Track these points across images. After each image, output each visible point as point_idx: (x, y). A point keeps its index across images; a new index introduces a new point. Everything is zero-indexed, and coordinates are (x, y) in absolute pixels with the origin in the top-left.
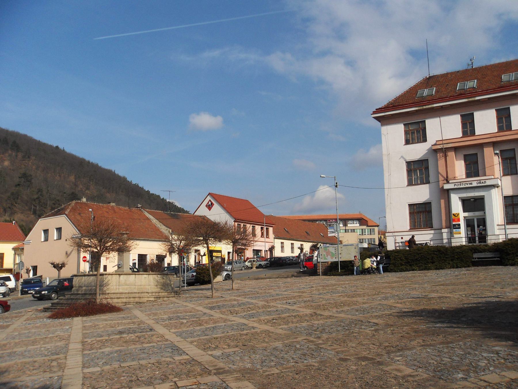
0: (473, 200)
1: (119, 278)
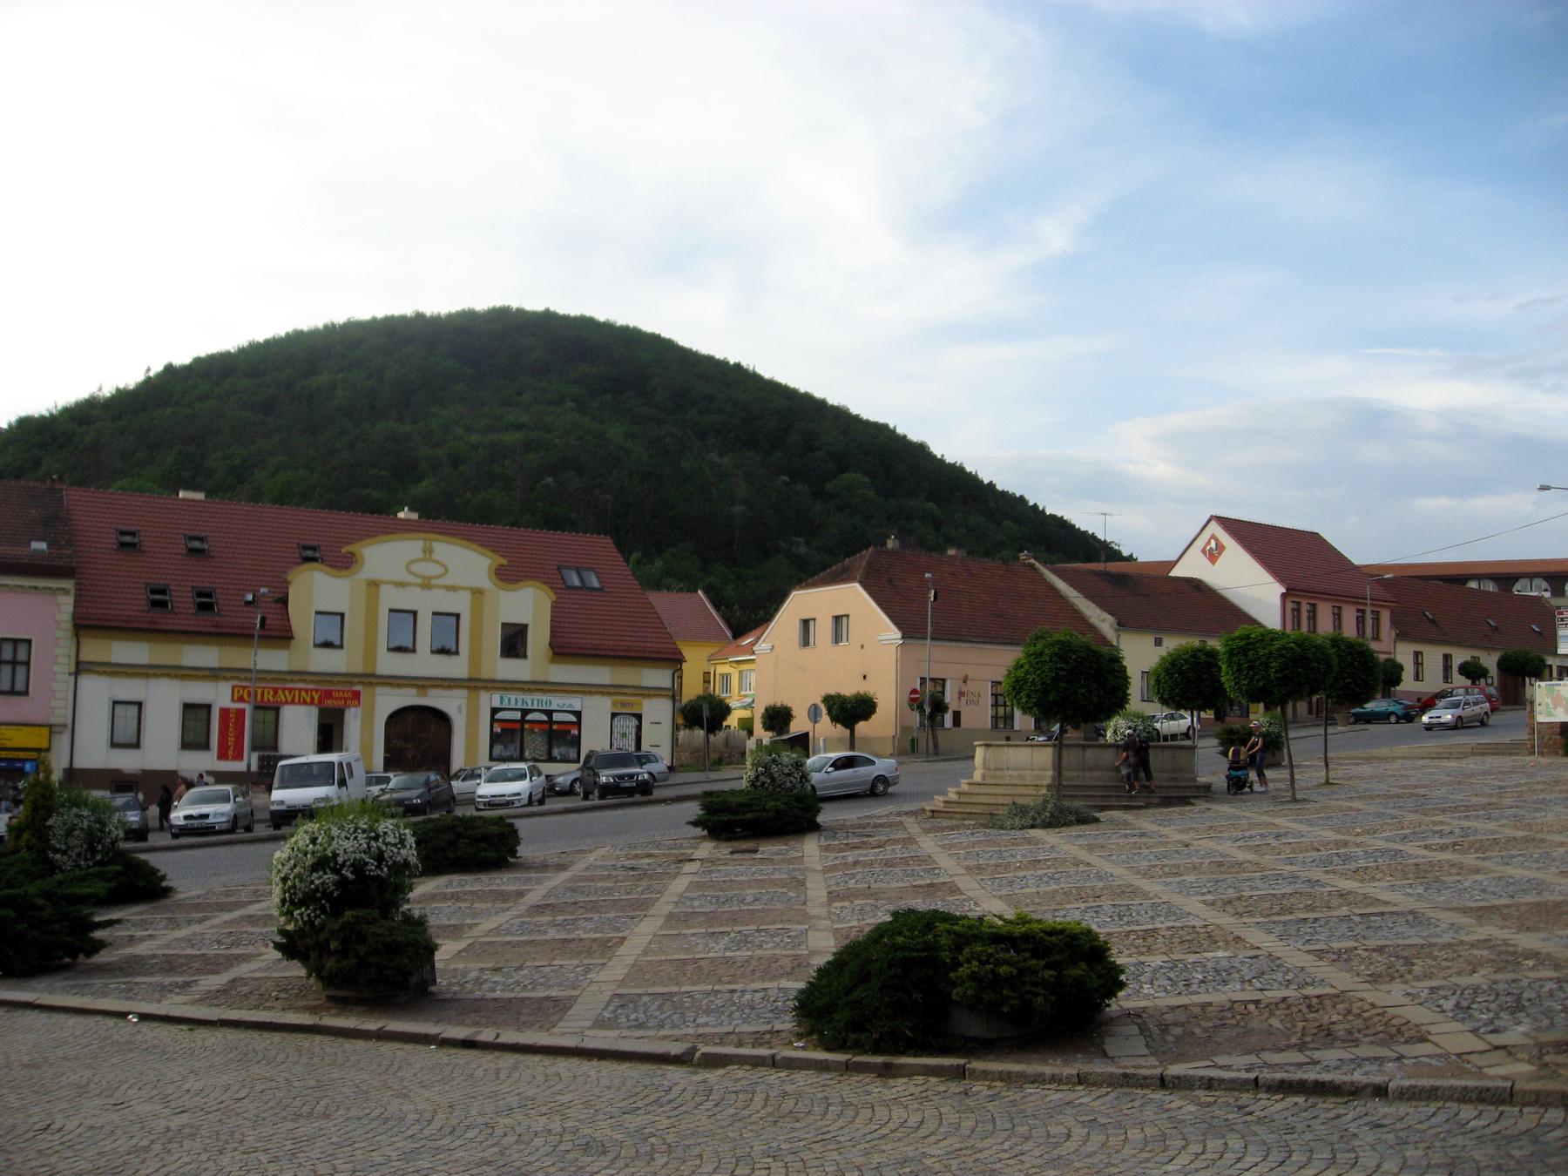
1: (1084, 754)
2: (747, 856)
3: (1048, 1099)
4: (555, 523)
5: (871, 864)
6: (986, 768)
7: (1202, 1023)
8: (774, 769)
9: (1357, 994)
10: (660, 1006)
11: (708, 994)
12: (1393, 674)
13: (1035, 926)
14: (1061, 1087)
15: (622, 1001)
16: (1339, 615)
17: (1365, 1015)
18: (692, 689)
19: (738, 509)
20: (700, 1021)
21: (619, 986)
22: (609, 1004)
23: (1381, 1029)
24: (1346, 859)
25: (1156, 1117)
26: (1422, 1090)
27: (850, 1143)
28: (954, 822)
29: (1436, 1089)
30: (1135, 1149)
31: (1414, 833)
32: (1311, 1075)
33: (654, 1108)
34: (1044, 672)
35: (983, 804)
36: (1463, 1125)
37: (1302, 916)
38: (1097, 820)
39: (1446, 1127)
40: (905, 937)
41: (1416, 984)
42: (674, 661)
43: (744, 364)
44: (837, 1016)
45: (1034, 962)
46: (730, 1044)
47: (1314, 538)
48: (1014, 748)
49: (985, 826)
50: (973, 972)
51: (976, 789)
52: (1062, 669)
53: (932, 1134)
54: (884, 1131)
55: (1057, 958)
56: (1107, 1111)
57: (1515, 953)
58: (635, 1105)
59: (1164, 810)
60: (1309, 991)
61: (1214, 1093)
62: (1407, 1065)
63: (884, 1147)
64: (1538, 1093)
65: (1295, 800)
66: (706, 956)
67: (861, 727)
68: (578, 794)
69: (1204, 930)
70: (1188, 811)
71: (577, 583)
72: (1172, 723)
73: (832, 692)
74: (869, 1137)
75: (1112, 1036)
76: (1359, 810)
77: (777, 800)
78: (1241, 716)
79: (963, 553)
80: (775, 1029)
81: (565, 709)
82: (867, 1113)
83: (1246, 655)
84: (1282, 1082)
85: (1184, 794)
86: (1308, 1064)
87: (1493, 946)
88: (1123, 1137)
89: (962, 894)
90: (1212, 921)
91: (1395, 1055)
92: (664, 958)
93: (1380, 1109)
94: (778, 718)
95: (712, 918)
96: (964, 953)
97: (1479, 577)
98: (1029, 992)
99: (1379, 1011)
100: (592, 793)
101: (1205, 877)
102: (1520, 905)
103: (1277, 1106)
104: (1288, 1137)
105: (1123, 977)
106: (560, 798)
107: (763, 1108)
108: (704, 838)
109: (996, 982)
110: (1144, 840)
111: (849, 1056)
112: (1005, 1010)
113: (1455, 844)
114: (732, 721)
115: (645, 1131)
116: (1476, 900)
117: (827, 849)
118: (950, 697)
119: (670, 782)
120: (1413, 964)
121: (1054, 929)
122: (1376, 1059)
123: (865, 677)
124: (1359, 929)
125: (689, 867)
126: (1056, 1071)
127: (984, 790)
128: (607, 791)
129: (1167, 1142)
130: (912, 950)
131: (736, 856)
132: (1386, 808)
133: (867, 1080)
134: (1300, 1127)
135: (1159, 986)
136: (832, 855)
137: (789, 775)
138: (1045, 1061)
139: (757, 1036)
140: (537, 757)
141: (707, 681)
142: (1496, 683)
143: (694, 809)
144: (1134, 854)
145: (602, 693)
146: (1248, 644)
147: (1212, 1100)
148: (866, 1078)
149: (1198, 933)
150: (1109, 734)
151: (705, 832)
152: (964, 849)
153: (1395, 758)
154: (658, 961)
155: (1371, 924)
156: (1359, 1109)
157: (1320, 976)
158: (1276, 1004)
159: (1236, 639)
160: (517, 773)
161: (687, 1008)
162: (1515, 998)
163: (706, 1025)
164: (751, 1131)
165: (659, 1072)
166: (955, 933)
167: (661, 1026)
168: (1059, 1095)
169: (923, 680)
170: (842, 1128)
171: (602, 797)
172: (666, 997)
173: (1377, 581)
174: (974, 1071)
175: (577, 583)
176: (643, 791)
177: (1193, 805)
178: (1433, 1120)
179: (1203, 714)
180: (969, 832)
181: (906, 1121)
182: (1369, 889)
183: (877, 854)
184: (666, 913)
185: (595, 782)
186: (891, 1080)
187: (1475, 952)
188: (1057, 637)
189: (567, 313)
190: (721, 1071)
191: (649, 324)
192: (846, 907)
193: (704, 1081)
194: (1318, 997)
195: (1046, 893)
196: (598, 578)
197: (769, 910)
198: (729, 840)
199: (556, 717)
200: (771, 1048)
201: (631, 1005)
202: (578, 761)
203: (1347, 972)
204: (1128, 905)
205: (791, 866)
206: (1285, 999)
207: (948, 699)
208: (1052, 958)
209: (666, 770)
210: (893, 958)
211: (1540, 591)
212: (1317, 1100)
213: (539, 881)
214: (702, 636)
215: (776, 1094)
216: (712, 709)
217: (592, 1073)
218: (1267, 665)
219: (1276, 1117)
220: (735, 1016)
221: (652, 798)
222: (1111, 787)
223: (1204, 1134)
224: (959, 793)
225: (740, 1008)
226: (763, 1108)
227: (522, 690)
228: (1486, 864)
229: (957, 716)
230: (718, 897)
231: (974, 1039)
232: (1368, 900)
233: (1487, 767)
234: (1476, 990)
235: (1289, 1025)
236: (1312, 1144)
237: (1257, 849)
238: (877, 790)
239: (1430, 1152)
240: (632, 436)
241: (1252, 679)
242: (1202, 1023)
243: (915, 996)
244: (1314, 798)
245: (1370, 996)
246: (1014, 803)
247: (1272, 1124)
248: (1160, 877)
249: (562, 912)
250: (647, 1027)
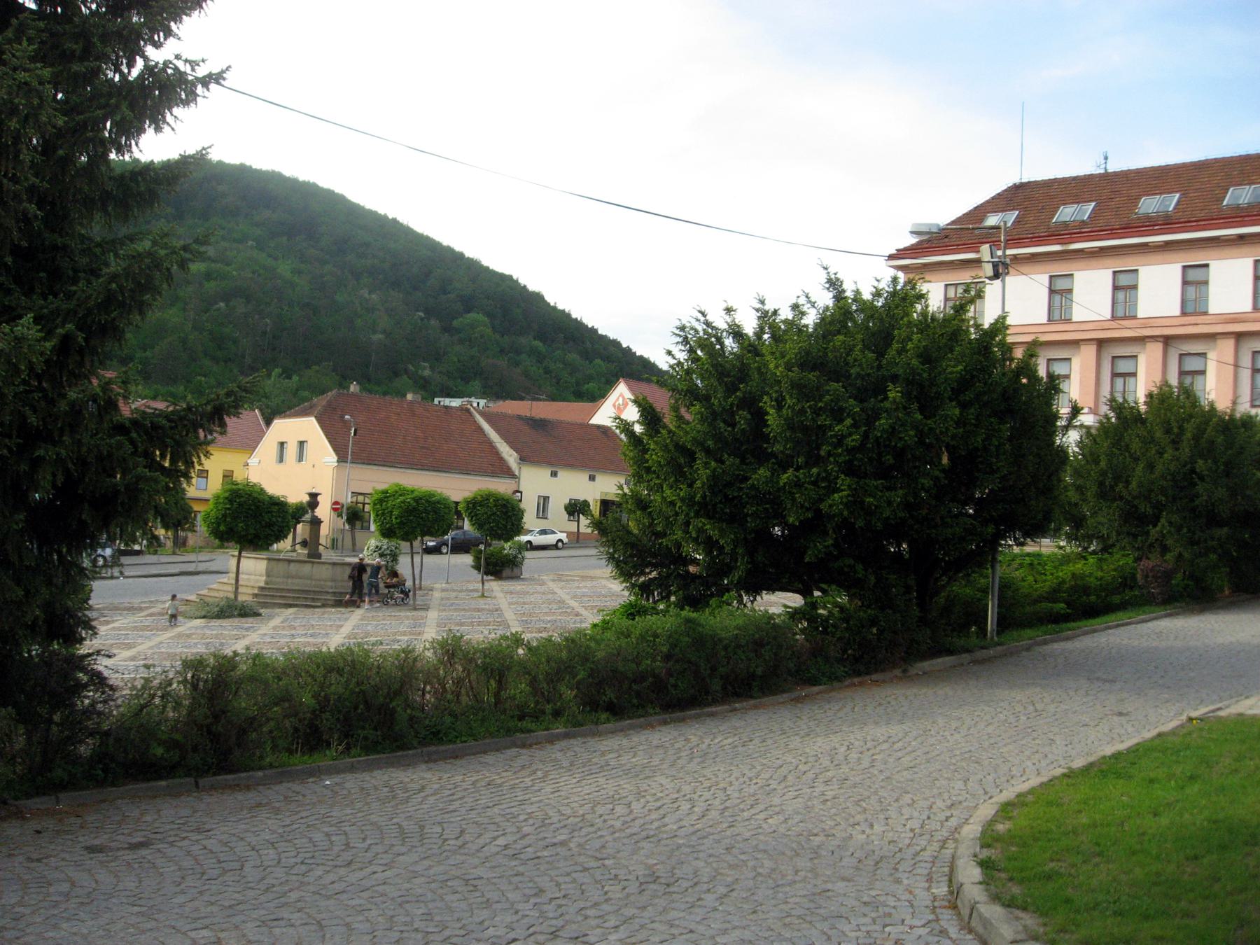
38: (259, 615)
213: (149, 638)
240: (300, 272)
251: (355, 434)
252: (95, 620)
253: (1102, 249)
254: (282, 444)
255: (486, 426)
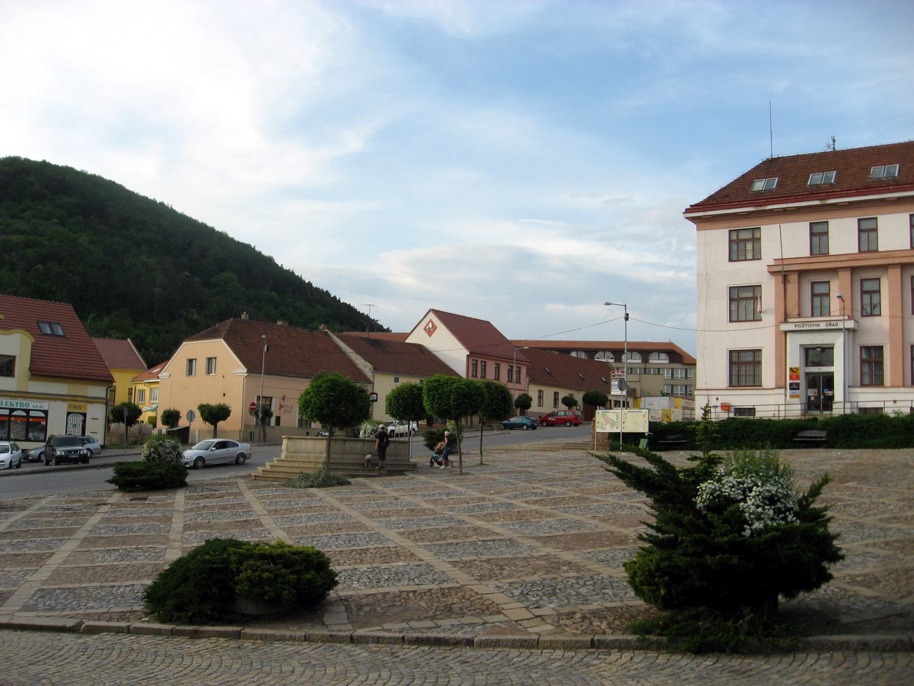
0: (820, 349)
1: (344, 444)
2: (141, 502)
3: (287, 650)
4: (42, 295)
5: (213, 508)
6: (288, 451)
7: (382, 604)
8: (161, 449)
9: (469, 587)
10: (66, 596)
11: (97, 588)
12: (524, 403)
13: (286, 549)
14: (295, 643)
15: (43, 593)
16: (499, 368)
17: (472, 599)
18: (121, 398)
19: (158, 290)
20: (89, 605)
21: (43, 584)
22: (34, 595)
23: (478, 607)
24: (482, 508)
25: (345, 660)
26: (492, 641)
27: (164, 679)
28: (267, 483)
29: (499, 641)
30: (328, 679)
31: (522, 494)
32: (433, 634)
33: (49, 661)
34: (321, 397)
35: (285, 472)
36: (510, 661)
37: (450, 541)
38: (349, 483)
39: (501, 662)
40: (211, 555)
41: (503, 581)
42: (108, 381)
43: (166, 203)
44: (168, 603)
45: (284, 570)
46: (103, 620)
47: (488, 323)
48: (304, 440)
49: (284, 485)
50: (248, 577)
51: (281, 464)
52: (332, 396)
53: (215, 672)
54: (186, 672)
55: (298, 568)
56: (318, 657)
57: (559, 562)
58: (38, 659)
59: (388, 478)
60: (445, 585)
61: (380, 645)
62: (487, 628)
63: (184, 681)
64: (551, 642)
65: (462, 474)
66: (100, 564)
67: (221, 424)
68: (43, 461)
69: (394, 549)
70: (402, 479)
71: (49, 331)
72: (401, 427)
73: (204, 403)
74: (176, 676)
75: (329, 612)
76: (495, 480)
77: (162, 468)
78: (442, 423)
79: (287, 324)
80: (133, 610)
81: (38, 409)
82: (179, 660)
83: (438, 391)
84: (417, 638)
85: (403, 468)
86: (434, 627)
87: (549, 559)
88: (323, 672)
89: (262, 526)
90: (400, 544)
91: (482, 621)
92: (75, 566)
93: (468, 652)
94: (171, 417)
95: (111, 541)
96: (244, 565)
97: (577, 350)
98: (281, 588)
99: (479, 596)
100: (51, 461)
101: (402, 518)
102: (568, 535)
103: (412, 653)
104: (415, 670)
105: (337, 579)
106: (31, 464)
107: (117, 659)
108: (115, 490)
109: (261, 582)
110: (374, 495)
111: (174, 626)
112: (266, 598)
113: (542, 500)
114: (144, 417)
115: (42, 675)
116: (546, 532)
117: (189, 498)
118: (274, 408)
119: (102, 454)
120: (504, 569)
121: (297, 551)
122: (471, 624)
123: (224, 395)
124: (480, 549)
125: (104, 509)
126: (293, 633)
127: (286, 464)
128: (60, 460)
129: (348, 675)
130: (214, 563)
131: (133, 502)
132: (510, 479)
133: (183, 640)
134: (423, 664)
135: (362, 583)
136: (192, 502)
137: (169, 453)
138: (278, 629)
139: (121, 614)
140: (19, 438)
141: (130, 394)
142: (581, 409)
143: (110, 473)
144: (366, 504)
145: (62, 400)
146: (439, 385)
147: (377, 649)
148: (182, 639)
149: (391, 551)
150: (361, 433)
151: (117, 487)
152: (269, 500)
153: (520, 450)
154: (70, 568)
155: (487, 546)
156: (456, 653)
157: (452, 576)
158: (425, 593)
159: (432, 381)
160: (5, 448)
161: (83, 597)
162: (552, 588)
163: (92, 608)
164: (106, 673)
165: (58, 638)
166: (240, 554)
167: (64, 609)
168: (293, 648)
169: (258, 398)
170: (162, 670)
171: (57, 464)
172: (71, 590)
173: (520, 350)
174: (246, 634)
175: (49, 331)
176: (83, 460)
177: (406, 475)
178: (495, 658)
179: (420, 422)
180: (275, 489)
181: (200, 665)
182: (491, 526)
183: (218, 502)
184: (83, 537)
185: (53, 455)
186: (197, 640)
187: (538, 562)
188: (330, 377)
189: (57, 164)
190: (96, 636)
191: (108, 175)
192: (192, 534)
193: (85, 643)
194: (448, 589)
195: (311, 527)
196: (63, 329)
197: (146, 535)
198: (130, 492)
199: (32, 414)
200: (128, 622)
201: (48, 596)
202: (44, 441)
203: (468, 574)
204: (355, 534)
205: (165, 509)
206: (430, 590)
207: (273, 409)
208: (295, 568)
209: (99, 447)
210: (203, 568)
211: (609, 359)
212: (435, 648)
213: (7, 517)
214: (125, 367)
215: (126, 650)
216: (130, 411)
217: (16, 639)
218: (449, 397)
219: (411, 659)
220: (111, 602)
221: (88, 465)
222: (356, 464)
223: (369, 670)
224: (272, 466)
225: (116, 597)
226: (117, 659)
227: (10, 396)
228: (556, 512)
229: (278, 419)
230: (117, 528)
231: (248, 615)
232: (489, 532)
233: (568, 456)
234: (534, 584)
235: (429, 605)
236: (427, 674)
237: (435, 502)
238: (239, 461)
239: (489, 676)
241: (440, 405)
242: (382, 604)
243: (214, 590)
244: (472, 472)
245: (476, 588)
246: (302, 473)
247: (408, 663)
248: (378, 518)
249: (18, 537)
250: (56, 610)
251: (267, 350)
252: (121, 497)
253: (850, 203)
254: (191, 361)
255: (342, 345)
